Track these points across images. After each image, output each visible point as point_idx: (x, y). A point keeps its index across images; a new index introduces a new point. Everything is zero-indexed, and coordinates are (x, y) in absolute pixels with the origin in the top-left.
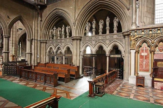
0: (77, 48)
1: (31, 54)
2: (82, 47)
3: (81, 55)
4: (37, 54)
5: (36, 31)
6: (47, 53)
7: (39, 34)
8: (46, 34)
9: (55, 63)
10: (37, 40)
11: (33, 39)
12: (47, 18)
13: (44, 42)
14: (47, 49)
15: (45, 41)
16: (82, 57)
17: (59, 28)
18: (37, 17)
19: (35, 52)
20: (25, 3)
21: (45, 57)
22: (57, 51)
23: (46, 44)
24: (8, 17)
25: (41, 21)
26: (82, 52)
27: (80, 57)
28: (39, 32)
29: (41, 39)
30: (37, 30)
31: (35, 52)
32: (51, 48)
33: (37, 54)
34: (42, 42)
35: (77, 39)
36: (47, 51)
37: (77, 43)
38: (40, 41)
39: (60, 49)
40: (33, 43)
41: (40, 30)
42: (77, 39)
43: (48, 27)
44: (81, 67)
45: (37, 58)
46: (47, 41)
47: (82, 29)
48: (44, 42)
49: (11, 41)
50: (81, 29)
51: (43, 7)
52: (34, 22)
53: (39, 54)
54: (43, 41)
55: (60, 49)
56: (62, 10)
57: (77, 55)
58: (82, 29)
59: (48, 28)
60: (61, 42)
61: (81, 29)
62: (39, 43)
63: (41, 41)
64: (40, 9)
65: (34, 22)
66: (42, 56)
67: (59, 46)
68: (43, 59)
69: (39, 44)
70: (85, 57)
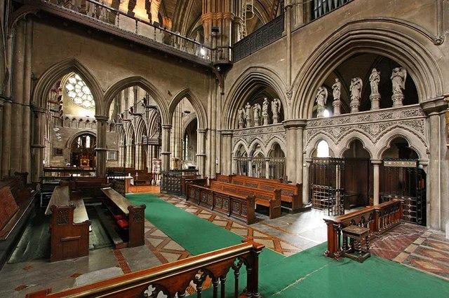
3: (305, 160)
4: (215, 157)
5: (213, 114)
6: (233, 156)
7: (218, 119)
10: (215, 130)
11: (207, 129)
14: (233, 145)
16: (309, 164)
21: (229, 163)
22: (253, 152)
24: (169, 93)
25: (223, 94)
26: (308, 153)
27: (304, 165)
28: (219, 114)
29: (223, 129)
32: (241, 146)
33: (215, 157)
34: (224, 134)
36: (234, 151)
39: (259, 147)
40: (208, 137)
45: (216, 164)
47: (306, 104)
48: (227, 134)
50: (305, 102)
51: (226, 67)
52: (209, 98)
53: (219, 157)
58: (306, 104)
59: (235, 106)
60: (261, 133)
61: (305, 102)
62: (218, 135)
63: (223, 133)
64: (220, 72)
65: (209, 98)
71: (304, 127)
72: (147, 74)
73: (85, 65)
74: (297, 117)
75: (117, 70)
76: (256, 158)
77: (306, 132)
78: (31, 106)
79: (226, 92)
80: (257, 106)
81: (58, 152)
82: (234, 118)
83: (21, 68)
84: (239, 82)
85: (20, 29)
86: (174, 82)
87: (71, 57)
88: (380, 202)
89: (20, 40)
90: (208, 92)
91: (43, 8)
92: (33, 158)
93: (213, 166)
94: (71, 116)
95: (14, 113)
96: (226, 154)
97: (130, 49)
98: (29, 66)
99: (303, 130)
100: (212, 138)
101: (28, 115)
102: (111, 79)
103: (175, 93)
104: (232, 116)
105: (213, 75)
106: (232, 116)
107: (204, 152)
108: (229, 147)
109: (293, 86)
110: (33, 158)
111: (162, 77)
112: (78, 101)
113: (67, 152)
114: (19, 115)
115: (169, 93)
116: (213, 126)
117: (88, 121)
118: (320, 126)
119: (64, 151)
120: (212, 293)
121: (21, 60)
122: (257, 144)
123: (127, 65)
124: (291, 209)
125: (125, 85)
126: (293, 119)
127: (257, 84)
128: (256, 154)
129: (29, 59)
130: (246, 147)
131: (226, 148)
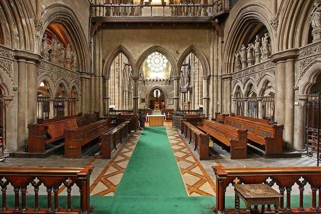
0: (284, 82)
1: (208, 99)
2: (300, 75)
3: (297, 98)
4: (217, 99)
5: (215, 62)
6: (233, 97)
7: (220, 65)
8: (231, 63)
9: (245, 116)
10: (217, 76)
11: (210, 76)
12: (229, 34)
13: (227, 78)
14: (232, 87)
15: (228, 76)
16: (302, 103)
17: (249, 45)
18: (216, 38)
19: (213, 96)
20: (139, 25)
21: (229, 104)
22: (263, 91)
23: (231, 80)
24: (177, 52)
25: (222, 42)
26: (301, 89)
27: (296, 103)
28: (220, 61)
29: (223, 74)
30: (217, 60)
31: (213, 96)
32: (239, 88)
33: (217, 99)
34: (224, 79)
35: (285, 59)
36: (233, 93)
37: (28, 68)
38: (222, 76)
39: (270, 87)
40: (211, 82)
41: (220, 58)
42: (285, 59)
43: (233, 48)
44: (298, 131)
45: (217, 105)
46: (231, 74)
47: (298, 30)
48: (227, 78)
49: (197, 83)
50: (295, 28)
51: (223, 18)
52: (211, 49)
53: (220, 99)
54: (225, 77)
55: (270, 87)
56: (250, 6)
57: (284, 99)
58: (298, 30)
59: (233, 50)
60: (254, 73)
61: (295, 28)
62: (220, 79)
63: (223, 77)
64: (219, 23)
65: (211, 49)
66: (224, 102)
67: (250, 81)
68: (226, 108)
69: (220, 82)
70: (310, 103)
71: (294, 58)
72: (161, 42)
73: (125, 47)
74: (285, 49)
75: (142, 45)
76: (267, 97)
77: (298, 64)
78: (102, 76)
79: (225, 40)
80: (251, 46)
81: (143, 100)
82: (233, 62)
83: (98, 57)
84: (233, 27)
85: (97, 36)
86: (181, 43)
87: (119, 44)
88: (264, 151)
89: (97, 42)
90: (210, 43)
91: (104, 21)
92: (104, 104)
93: (215, 107)
94: (148, 79)
95: (95, 81)
96: (226, 95)
97: (151, 28)
98: (101, 56)
99: (294, 62)
100: (214, 82)
101: (101, 81)
102: (139, 52)
103: (181, 52)
104: (231, 61)
105: (214, 28)
106: (231, 61)
107: (208, 95)
108: (229, 89)
109: (278, 14)
110: (104, 104)
111: (171, 41)
112: (152, 69)
113: (147, 100)
114: (97, 82)
115: (177, 52)
116: (215, 72)
117: (157, 80)
118: (316, 53)
119: (146, 100)
120: (34, 200)
121: (97, 52)
122: (267, 82)
123: (149, 39)
124: (264, 152)
125: (150, 51)
126: (280, 51)
127: (250, 24)
128: (266, 94)
129: (101, 52)
130: (242, 88)
131: (226, 90)
